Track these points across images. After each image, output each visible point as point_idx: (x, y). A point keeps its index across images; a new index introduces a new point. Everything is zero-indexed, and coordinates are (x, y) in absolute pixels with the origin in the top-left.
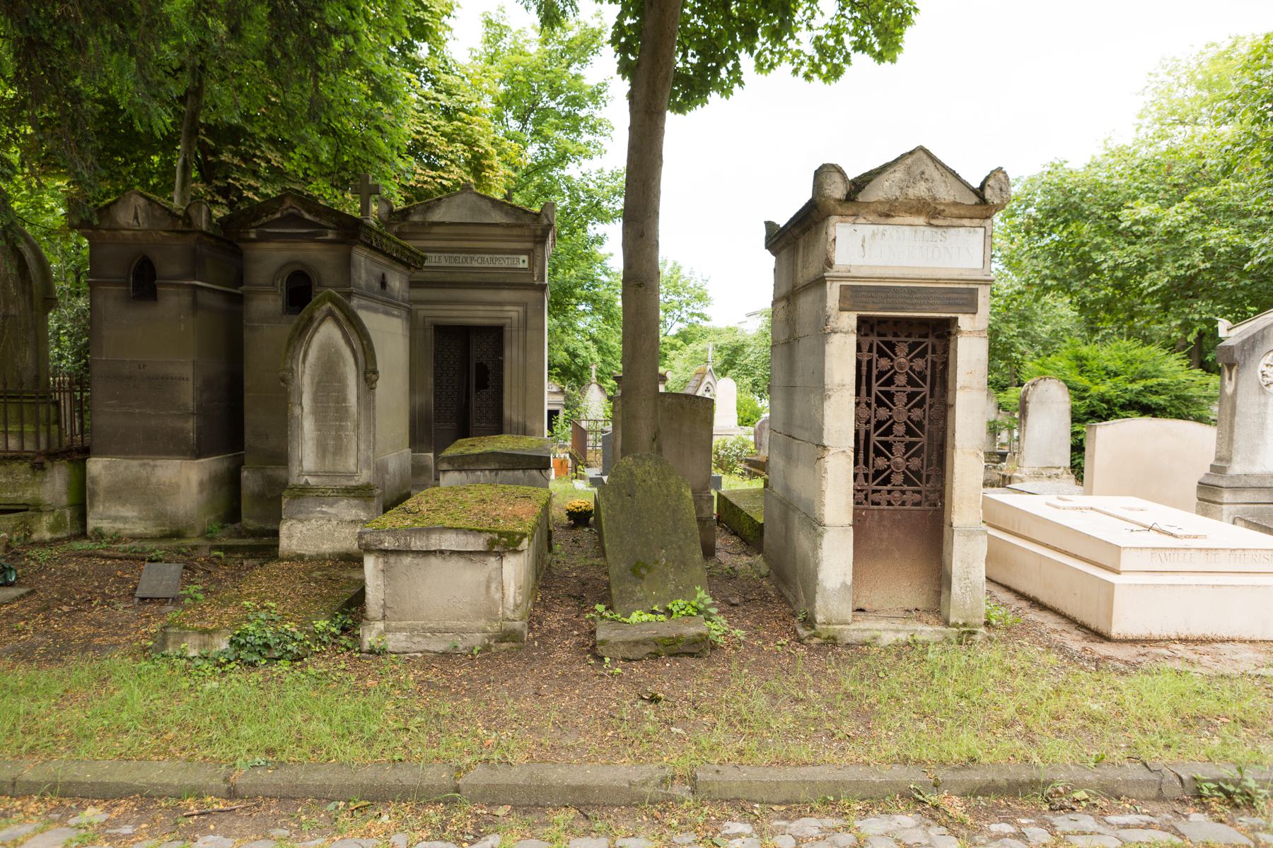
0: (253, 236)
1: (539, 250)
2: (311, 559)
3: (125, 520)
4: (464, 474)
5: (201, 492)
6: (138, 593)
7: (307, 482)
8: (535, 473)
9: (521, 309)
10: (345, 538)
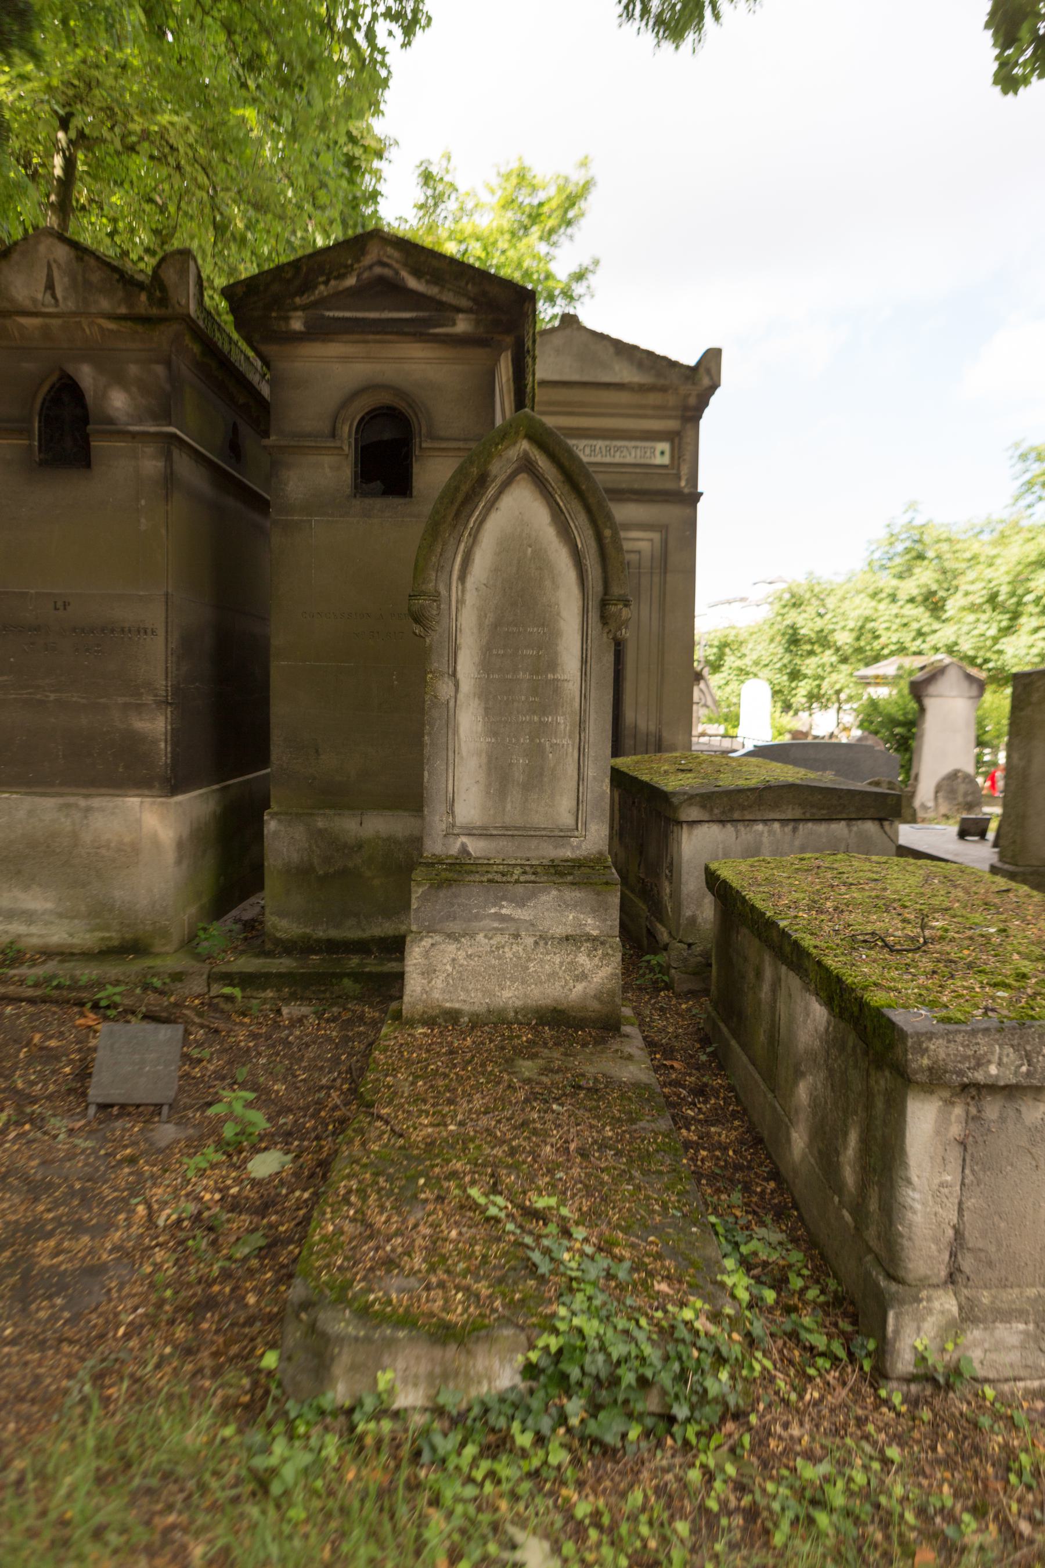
2: (477, 1022)
3: (29, 917)
4: (729, 827)
5: (179, 862)
6: (95, 1094)
7: (464, 850)
8: (870, 827)
9: (656, 536)
10: (553, 975)
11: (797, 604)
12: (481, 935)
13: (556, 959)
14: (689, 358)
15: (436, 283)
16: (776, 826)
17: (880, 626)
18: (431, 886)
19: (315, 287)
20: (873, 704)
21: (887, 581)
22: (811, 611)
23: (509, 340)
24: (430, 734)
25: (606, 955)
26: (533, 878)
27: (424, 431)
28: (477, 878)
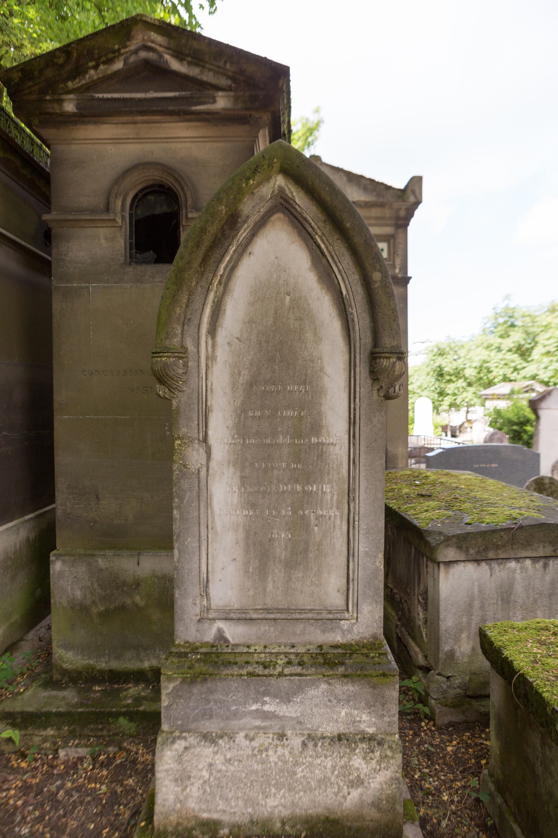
0: (70, 107)
1: (401, 236)
7: (221, 637)
10: (324, 781)
11: (442, 354)
12: (242, 734)
13: (327, 762)
14: (400, 183)
15: (197, 65)
16: (528, 562)
17: (492, 365)
18: (184, 680)
19: (86, 72)
20: (498, 412)
21: (496, 341)
22: (450, 357)
23: (266, 117)
24: (179, 507)
25: (384, 757)
26: (299, 670)
27: (190, 202)
28: (235, 670)
